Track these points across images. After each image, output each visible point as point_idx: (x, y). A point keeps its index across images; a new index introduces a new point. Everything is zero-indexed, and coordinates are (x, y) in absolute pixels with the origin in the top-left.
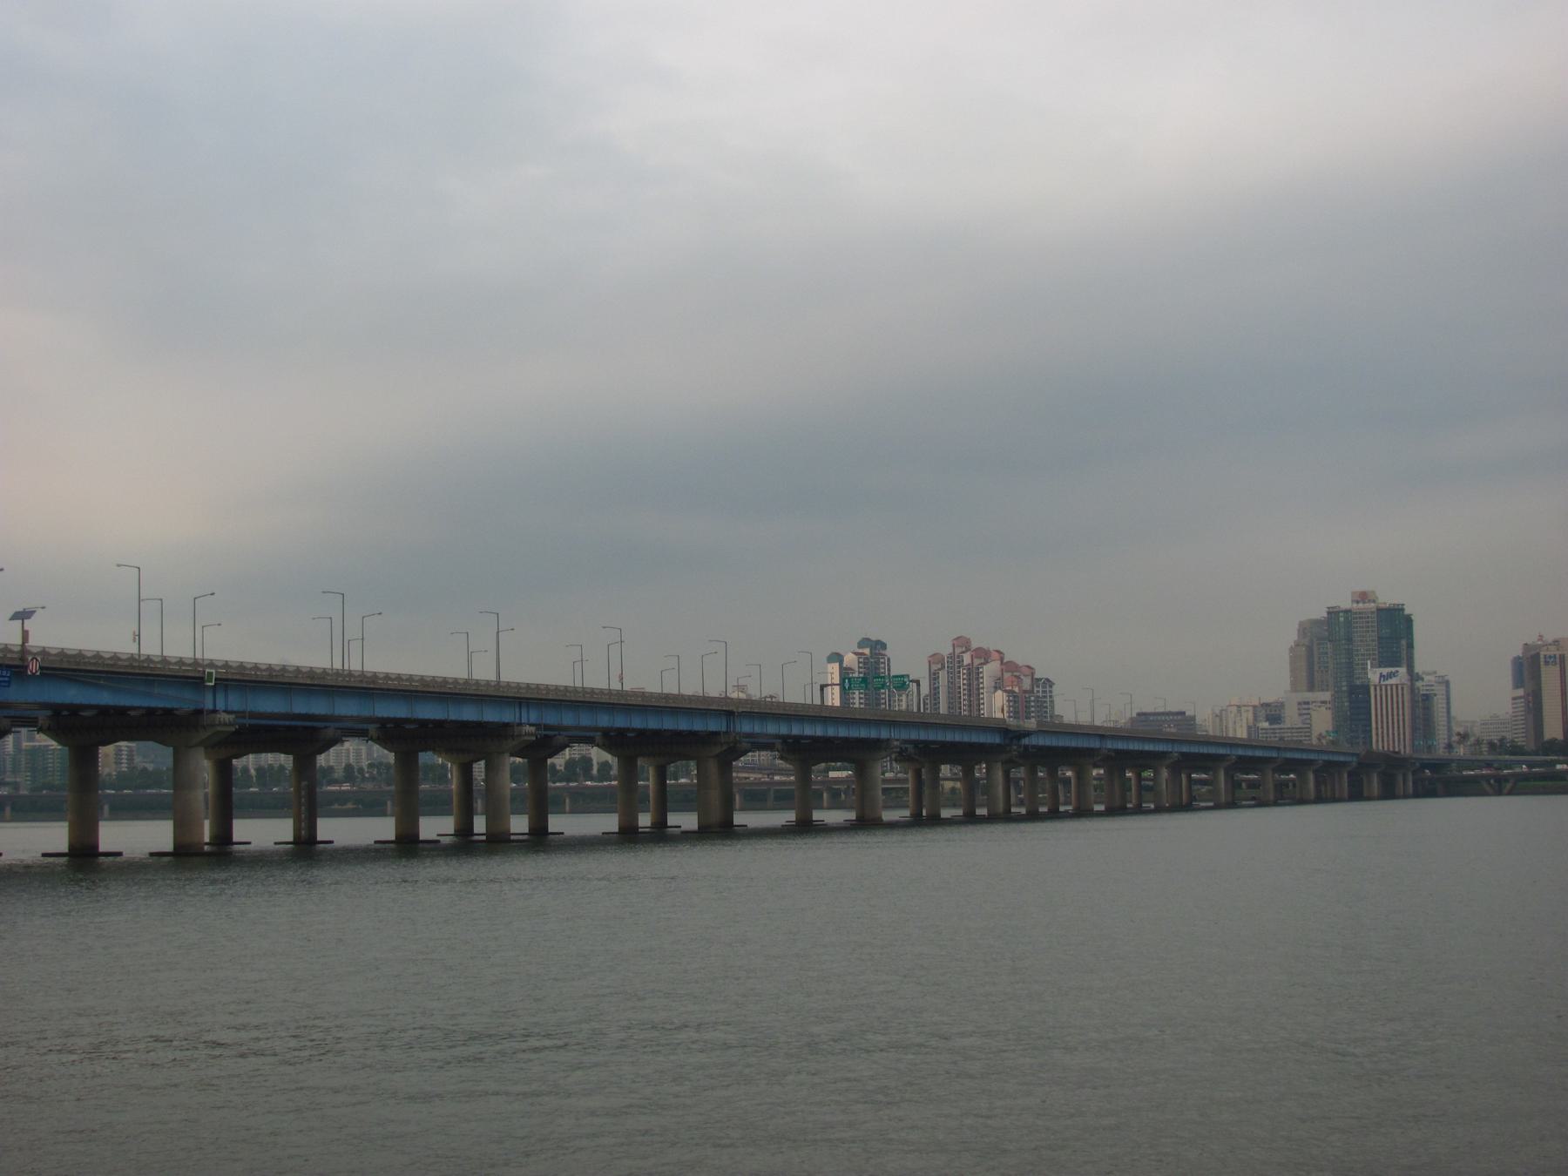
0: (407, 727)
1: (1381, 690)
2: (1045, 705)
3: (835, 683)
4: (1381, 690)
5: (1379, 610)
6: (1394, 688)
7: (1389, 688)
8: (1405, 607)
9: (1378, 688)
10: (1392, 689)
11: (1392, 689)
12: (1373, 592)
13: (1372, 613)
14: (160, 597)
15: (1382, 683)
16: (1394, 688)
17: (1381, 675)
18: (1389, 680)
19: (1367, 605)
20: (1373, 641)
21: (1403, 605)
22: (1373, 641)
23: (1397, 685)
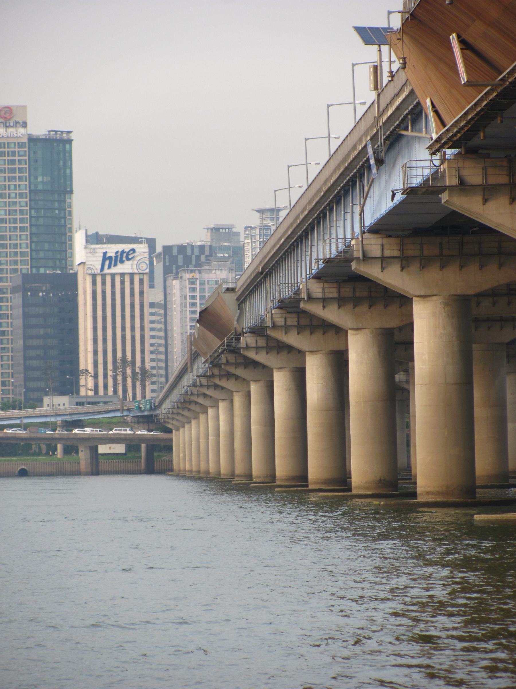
0: (512, 610)
1: (104, 283)
2: (154, 356)
3: (287, 322)
4: (104, 283)
5: (32, 140)
6: (127, 279)
7: (118, 279)
8: (72, 136)
9: (99, 279)
10: (123, 283)
11: (123, 283)
12: (24, 107)
13: (21, 145)
14: (304, 140)
15: (106, 271)
16: (127, 279)
17: (105, 257)
18: (119, 266)
19: (11, 131)
20: (21, 195)
21: (70, 132)
22: (21, 195)
23: (132, 275)
